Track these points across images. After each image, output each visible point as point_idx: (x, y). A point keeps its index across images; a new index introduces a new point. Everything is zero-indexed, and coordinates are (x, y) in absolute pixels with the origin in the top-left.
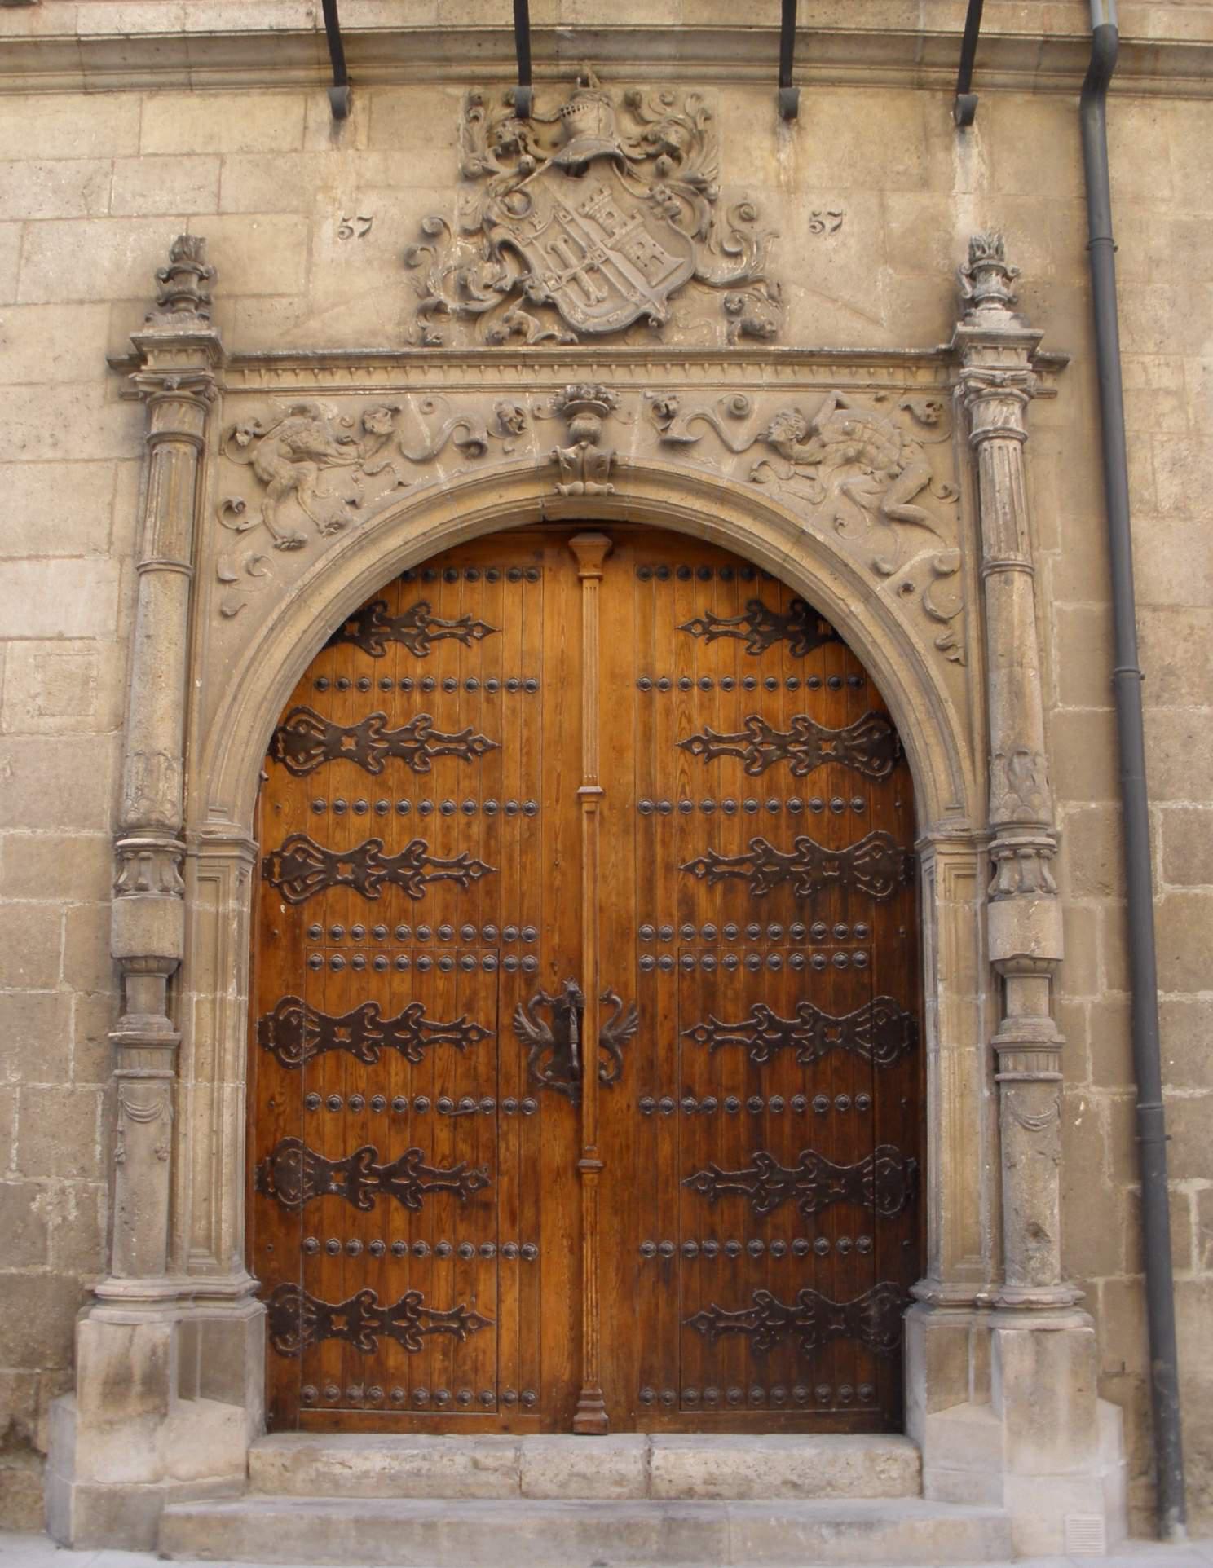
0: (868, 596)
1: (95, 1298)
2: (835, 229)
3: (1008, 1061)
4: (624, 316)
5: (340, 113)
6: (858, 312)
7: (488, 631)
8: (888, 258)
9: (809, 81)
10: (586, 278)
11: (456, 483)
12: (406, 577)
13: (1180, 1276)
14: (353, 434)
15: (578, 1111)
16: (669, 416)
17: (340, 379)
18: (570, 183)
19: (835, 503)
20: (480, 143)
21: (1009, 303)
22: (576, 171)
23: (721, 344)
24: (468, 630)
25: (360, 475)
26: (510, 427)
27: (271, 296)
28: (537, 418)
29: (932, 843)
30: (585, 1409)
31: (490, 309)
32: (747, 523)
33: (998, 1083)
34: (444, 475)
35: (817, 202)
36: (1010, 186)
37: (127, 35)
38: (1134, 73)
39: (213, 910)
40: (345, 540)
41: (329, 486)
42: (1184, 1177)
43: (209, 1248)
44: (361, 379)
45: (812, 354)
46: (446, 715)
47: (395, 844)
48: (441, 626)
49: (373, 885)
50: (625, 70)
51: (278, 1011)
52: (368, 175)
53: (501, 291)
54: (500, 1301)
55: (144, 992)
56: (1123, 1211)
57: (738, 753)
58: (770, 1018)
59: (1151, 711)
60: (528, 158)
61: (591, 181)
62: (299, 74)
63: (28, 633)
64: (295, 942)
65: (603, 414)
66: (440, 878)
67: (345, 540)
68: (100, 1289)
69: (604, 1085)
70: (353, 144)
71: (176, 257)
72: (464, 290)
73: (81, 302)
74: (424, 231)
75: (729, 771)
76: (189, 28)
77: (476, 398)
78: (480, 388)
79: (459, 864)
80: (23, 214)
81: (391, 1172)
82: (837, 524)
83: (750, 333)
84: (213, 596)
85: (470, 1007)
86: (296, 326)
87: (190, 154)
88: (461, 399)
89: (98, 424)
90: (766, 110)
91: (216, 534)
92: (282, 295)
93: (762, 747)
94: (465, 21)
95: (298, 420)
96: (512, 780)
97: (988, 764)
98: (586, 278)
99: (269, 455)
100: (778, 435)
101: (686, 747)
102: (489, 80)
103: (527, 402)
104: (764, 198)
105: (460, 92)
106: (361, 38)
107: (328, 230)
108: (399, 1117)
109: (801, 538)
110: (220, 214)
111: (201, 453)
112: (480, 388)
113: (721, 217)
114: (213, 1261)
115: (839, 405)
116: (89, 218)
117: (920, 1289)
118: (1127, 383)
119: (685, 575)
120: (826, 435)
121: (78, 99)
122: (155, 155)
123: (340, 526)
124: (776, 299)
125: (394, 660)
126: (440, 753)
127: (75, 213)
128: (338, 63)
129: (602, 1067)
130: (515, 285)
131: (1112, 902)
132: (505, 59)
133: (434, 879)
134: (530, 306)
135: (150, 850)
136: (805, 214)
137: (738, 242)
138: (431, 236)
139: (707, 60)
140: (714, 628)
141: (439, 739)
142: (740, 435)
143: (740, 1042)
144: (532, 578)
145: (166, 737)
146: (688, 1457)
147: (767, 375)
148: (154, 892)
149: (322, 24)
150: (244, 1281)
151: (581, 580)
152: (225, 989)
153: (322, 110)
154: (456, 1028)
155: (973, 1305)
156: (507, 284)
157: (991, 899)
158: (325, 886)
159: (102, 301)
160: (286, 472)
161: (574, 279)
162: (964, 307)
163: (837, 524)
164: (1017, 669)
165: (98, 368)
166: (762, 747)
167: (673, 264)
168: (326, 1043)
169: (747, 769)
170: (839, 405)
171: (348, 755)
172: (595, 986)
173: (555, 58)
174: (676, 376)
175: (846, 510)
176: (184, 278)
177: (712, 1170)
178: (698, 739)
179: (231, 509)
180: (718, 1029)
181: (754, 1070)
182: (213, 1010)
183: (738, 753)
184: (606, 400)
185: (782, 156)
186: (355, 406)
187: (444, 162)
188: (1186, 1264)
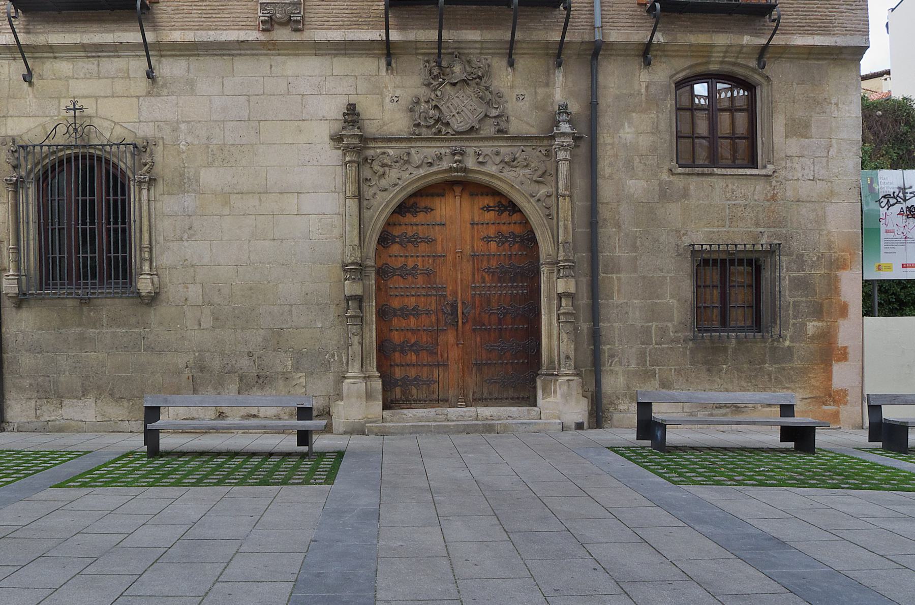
4: (468, 127)
5: (389, 64)
6: (528, 124)
8: (537, 108)
12: (411, 196)
13: (603, 369)
14: (398, 159)
15: (457, 330)
16: (479, 155)
19: (521, 178)
21: (569, 122)
22: (454, 84)
26: (440, 158)
31: (431, 124)
32: (499, 183)
34: (422, 172)
36: (570, 85)
38: (606, 50)
40: (397, 189)
41: (393, 174)
46: (421, 231)
47: (410, 263)
56: (589, 353)
59: (600, 230)
61: (458, 86)
64: (386, 291)
65: (462, 155)
67: (397, 189)
75: (493, 245)
77: (429, 151)
81: (412, 346)
85: (430, 305)
88: (425, 150)
90: (504, 62)
91: (365, 187)
93: (502, 239)
96: (439, 248)
99: (376, 167)
103: (443, 151)
104: (504, 91)
108: (413, 331)
118: (599, 142)
119: (482, 195)
121: (314, 57)
123: (396, 185)
124: (507, 121)
125: (409, 218)
131: (589, 278)
132: (434, 48)
135: (356, 270)
138: (418, 102)
142: (498, 159)
144: (443, 196)
145: (356, 242)
146: (486, 411)
149: (384, 38)
153: (383, 62)
156: (436, 118)
160: (381, 170)
162: (557, 124)
165: (327, 139)
166: (502, 239)
167: (481, 110)
168: (395, 315)
176: (352, 114)
181: (500, 319)
186: (398, 152)
188: (604, 365)
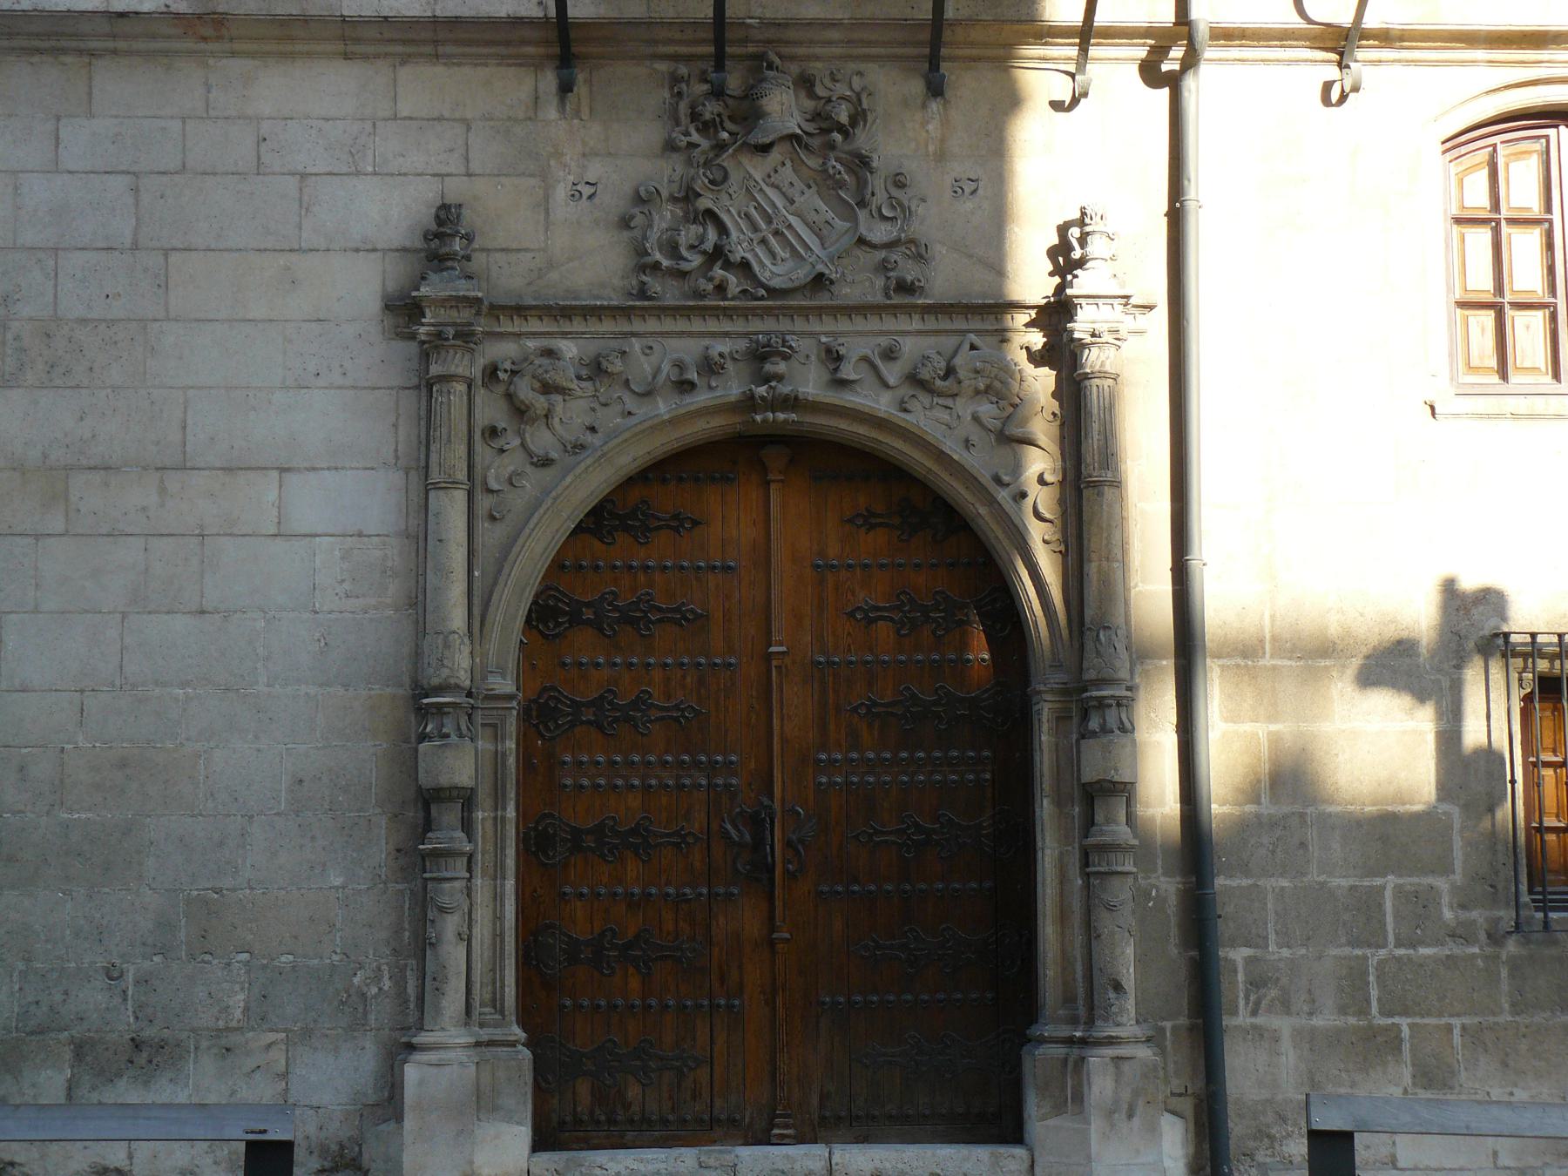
0: (992, 502)
1: (411, 1048)
2: (974, 192)
3: (1094, 858)
4: (802, 274)
5: (565, 88)
7: (695, 523)
9: (952, 59)
10: (772, 240)
11: (674, 413)
13: (1227, 1021)
15: (771, 898)
17: (577, 325)
18: (758, 159)
20: (684, 120)
23: (879, 298)
24: (680, 523)
25: (597, 406)
27: (519, 250)
28: (734, 359)
29: (1039, 692)
30: (779, 1127)
33: (1088, 874)
34: (663, 407)
35: (958, 169)
37: (386, 17)
39: (492, 748)
41: (572, 414)
42: (1232, 946)
43: (495, 1007)
44: (594, 326)
45: (952, 305)
48: (659, 519)
49: (610, 724)
50: (801, 51)
51: (537, 823)
52: (592, 143)
53: (704, 253)
54: (712, 1042)
55: (449, 816)
57: (892, 620)
58: (916, 825)
60: (725, 135)
62: (530, 50)
63: (331, 531)
66: (663, 718)
68: (415, 1040)
69: (791, 876)
70: (577, 113)
71: (440, 221)
72: (673, 250)
73: (357, 250)
74: (637, 192)
76: (438, 13)
77: (683, 344)
78: (690, 334)
79: (677, 708)
80: (300, 168)
82: (968, 444)
83: (904, 287)
84: (484, 503)
86: (540, 278)
87: (440, 119)
89: (374, 357)
90: (917, 86)
92: (526, 250)
94: (671, 13)
95: (546, 361)
97: (1082, 633)
98: (772, 240)
100: (925, 374)
101: (851, 615)
102: (688, 58)
105: (662, 67)
106: (584, 25)
107: (561, 193)
109: (941, 456)
110: (469, 175)
111: (469, 387)
112: (690, 334)
113: (878, 185)
114: (497, 1017)
115: (973, 347)
116: (358, 173)
117: (1035, 1031)
120: (962, 374)
122: (411, 118)
124: (920, 254)
126: (660, 621)
127: (345, 169)
128: (564, 47)
129: (790, 862)
130: (716, 246)
132: (703, 41)
133: (657, 719)
134: (728, 265)
136: (949, 180)
137: (894, 208)
139: (869, 43)
140: (873, 521)
141: (659, 610)
142: (892, 373)
143: (894, 843)
147: (916, 324)
148: (454, 738)
149: (552, 13)
150: (518, 1033)
151: (768, 483)
152: (504, 809)
154: (677, 833)
155: (1070, 1041)
156: (709, 246)
157: (1083, 737)
158: (572, 725)
159: (374, 250)
160: (540, 402)
161: (763, 241)
163: (968, 444)
164: (1104, 563)
169: (898, 632)
170: (973, 347)
171: (588, 622)
172: (783, 799)
173: (745, 41)
174: (844, 325)
175: (976, 435)
176: (443, 238)
177: (874, 940)
178: (859, 608)
179: (493, 432)
180: (877, 832)
182: (495, 825)
183: (892, 620)
184: (790, 347)
185: (930, 127)
186: (592, 348)
187: (650, 133)
188: (1234, 1012)
